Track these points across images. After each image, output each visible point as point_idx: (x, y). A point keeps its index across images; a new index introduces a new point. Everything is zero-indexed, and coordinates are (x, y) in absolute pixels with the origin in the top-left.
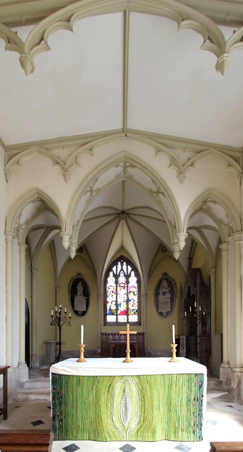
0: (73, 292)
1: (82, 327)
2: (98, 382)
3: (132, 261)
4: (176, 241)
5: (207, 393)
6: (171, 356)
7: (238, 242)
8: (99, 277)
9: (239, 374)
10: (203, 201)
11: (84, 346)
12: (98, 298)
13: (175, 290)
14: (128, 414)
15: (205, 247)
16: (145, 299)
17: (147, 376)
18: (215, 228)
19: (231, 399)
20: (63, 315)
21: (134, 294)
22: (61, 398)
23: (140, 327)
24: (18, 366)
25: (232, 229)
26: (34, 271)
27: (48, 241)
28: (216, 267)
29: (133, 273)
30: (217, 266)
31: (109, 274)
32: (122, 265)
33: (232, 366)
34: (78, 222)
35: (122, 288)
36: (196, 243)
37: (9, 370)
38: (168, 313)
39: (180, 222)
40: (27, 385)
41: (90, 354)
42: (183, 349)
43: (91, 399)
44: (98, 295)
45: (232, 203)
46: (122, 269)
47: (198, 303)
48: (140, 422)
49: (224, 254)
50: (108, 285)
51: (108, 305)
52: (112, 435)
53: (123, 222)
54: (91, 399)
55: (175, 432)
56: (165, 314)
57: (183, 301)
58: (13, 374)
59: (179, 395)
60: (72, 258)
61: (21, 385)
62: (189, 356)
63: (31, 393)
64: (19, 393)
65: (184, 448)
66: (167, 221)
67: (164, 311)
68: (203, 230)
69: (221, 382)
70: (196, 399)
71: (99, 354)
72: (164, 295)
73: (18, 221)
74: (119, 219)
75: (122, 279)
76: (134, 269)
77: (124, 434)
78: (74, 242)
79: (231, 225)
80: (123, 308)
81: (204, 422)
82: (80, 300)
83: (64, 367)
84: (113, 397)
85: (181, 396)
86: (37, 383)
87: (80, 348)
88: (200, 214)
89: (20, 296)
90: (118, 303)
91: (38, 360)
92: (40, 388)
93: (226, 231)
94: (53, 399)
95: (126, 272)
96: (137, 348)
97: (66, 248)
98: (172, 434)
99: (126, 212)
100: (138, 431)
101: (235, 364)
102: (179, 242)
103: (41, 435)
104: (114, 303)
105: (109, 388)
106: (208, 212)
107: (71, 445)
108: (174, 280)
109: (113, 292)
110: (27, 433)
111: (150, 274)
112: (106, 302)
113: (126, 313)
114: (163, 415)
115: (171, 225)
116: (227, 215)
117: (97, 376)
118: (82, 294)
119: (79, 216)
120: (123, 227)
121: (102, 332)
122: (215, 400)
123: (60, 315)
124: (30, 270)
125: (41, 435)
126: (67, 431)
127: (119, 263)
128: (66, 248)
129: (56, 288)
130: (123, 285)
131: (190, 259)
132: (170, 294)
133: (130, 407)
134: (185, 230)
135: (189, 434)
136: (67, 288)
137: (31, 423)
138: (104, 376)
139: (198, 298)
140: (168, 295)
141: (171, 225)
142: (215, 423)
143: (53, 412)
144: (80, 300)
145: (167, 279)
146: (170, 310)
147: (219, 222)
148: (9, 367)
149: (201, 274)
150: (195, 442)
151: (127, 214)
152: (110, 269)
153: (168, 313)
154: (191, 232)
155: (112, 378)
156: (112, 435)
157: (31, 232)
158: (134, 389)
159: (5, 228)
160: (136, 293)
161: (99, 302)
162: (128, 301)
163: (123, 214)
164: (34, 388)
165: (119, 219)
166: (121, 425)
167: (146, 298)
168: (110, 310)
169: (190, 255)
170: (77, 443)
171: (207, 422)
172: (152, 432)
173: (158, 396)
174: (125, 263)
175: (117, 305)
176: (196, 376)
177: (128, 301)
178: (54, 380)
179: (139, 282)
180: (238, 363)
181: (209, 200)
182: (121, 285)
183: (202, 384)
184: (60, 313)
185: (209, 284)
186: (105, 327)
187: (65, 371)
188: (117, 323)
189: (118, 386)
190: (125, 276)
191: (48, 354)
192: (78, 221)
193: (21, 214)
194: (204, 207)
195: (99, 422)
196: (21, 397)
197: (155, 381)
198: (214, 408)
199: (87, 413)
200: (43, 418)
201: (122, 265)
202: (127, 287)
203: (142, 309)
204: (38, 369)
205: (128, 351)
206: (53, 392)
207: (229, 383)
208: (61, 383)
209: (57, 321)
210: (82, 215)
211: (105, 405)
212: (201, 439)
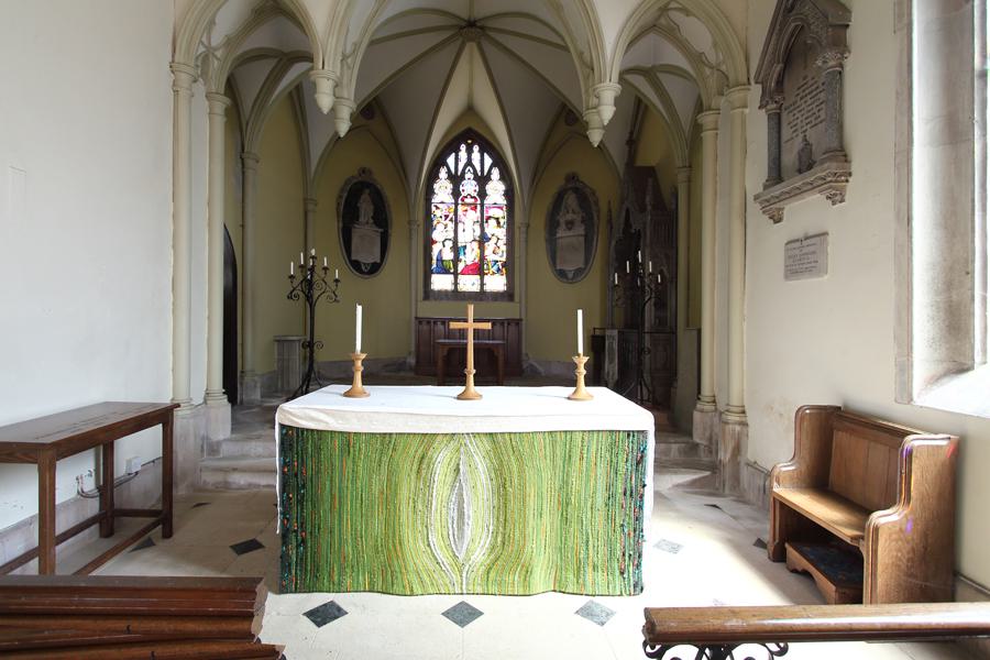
0: (348, 217)
1: (359, 308)
2: (394, 450)
3: (496, 146)
4: (594, 101)
5: (655, 471)
6: (572, 382)
7: (741, 110)
8: (413, 180)
9: (738, 428)
10: (660, 8)
11: (364, 356)
12: (410, 230)
13: (596, 218)
14: (466, 527)
15: (664, 114)
16: (524, 235)
17: (512, 436)
18: (686, 72)
19: (717, 489)
20: (319, 271)
21: (498, 223)
22: (304, 486)
23: (511, 304)
24: (205, 402)
25: (728, 79)
26: (249, 163)
27: (285, 88)
28: (690, 167)
29: (496, 173)
30: (692, 165)
31: (438, 172)
32: (470, 151)
33: (721, 407)
34: (356, 46)
35: (468, 208)
36: (646, 107)
37: (178, 413)
38: (579, 272)
39: (603, 57)
40: (225, 449)
41: (384, 373)
42: (611, 362)
43: (376, 489)
44: (409, 223)
45: (726, 17)
46: (469, 163)
47: (647, 251)
48: (493, 548)
49: (707, 136)
50: (436, 200)
51: (436, 249)
52: (427, 579)
53: (471, 50)
54: (376, 489)
55: (578, 572)
56: (570, 275)
57: (613, 243)
58: (191, 421)
59: (588, 481)
60: (342, 135)
61: (213, 449)
62: (620, 388)
63: (235, 470)
64: (207, 468)
65: (597, 611)
66: (572, 49)
67: (570, 268)
68: (659, 75)
69: (696, 446)
70: (628, 493)
71: (411, 369)
72: (570, 229)
73: (204, 39)
74: (461, 39)
75: (469, 187)
76: (499, 161)
77: (456, 578)
78: (346, 96)
79: (723, 68)
80: (470, 256)
81: (647, 549)
82: (365, 235)
83: (317, 410)
84: (429, 485)
85: (593, 483)
86: (253, 444)
87: (352, 363)
88: (651, 38)
89: (209, 225)
90: (460, 245)
91: (259, 385)
92: (259, 456)
93: (713, 81)
94: (283, 489)
95: (478, 168)
96: (501, 359)
97: (326, 110)
98: (571, 576)
99: (478, 24)
100: (491, 568)
101: (728, 405)
102: (599, 105)
103: (234, 591)
104: (449, 244)
105: (421, 462)
106: (672, 34)
107: (325, 605)
108: (594, 193)
109: (447, 217)
110: (199, 585)
111: (537, 176)
112: (429, 242)
113: (479, 269)
114: (548, 529)
115: (583, 63)
116: (715, 45)
117: (391, 434)
118: (371, 221)
119: (357, 30)
120: (471, 62)
121: (420, 315)
122: (680, 490)
123: (312, 274)
124: (240, 161)
125: (234, 591)
126: (316, 568)
127: (463, 148)
128: (326, 110)
129: (305, 204)
130: (472, 201)
131: (632, 143)
132: (583, 228)
133: (469, 510)
134: (615, 76)
135: (610, 578)
136: (335, 206)
137: (231, 547)
138: (409, 434)
139: (648, 241)
140: (580, 230)
141: (583, 63)
142: (675, 549)
143: (282, 522)
144: (365, 235)
145: (576, 190)
146: (583, 266)
147: (697, 58)
148: (178, 406)
149: (656, 180)
150: (625, 599)
151: (482, 28)
152: (439, 161)
153: (579, 272)
154: (629, 77)
155: (428, 438)
156: (427, 579)
157: (240, 65)
158: (481, 468)
159: (173, 56)
160: (502, 221)
161: (414, 242)
162: (483, 240)
163: (471, 29)
164: (244, 456)
165: (461, 39)
166: (449, 554)
167: (527, 233)
168: (440, 260)
169: (631, 133)
170: (340, 599)
171: (658, 546)
172: (524, 573)
173: (540, 483)
174: (476, 148)
175: (456, 249)
176: (629, 435)
177: (483, 240)
178: (286, 444)
179: (509, 194)
180: (735, 401)
181: (673, 5)
182: (467, 201)
183: (642, 457)
184: (312, 270)
185: (674, 207)
186: (427, 302)
187: (312, 419)
188: (456, 295)
189: (442, 461)
190: (476, 178)
191: (283, 370)
192: (355, 44)
193: (212, 23)
194: (663, 21)
195: (394, 546)
196: (210, 478)
197: (532, 445)
198: (677, 511)
199: (367, 525)
200: (261, 532)
201: (470, 151)
202: (482, 205)
203: (517, 260)
204: (260, 406)
205: (471, 370)
206: (283, 473)
207: (714, 447)
208: (304, 450)
209: (306, 288)
210: (369, 22)
211: (411, 504)
212: (638, 589)
